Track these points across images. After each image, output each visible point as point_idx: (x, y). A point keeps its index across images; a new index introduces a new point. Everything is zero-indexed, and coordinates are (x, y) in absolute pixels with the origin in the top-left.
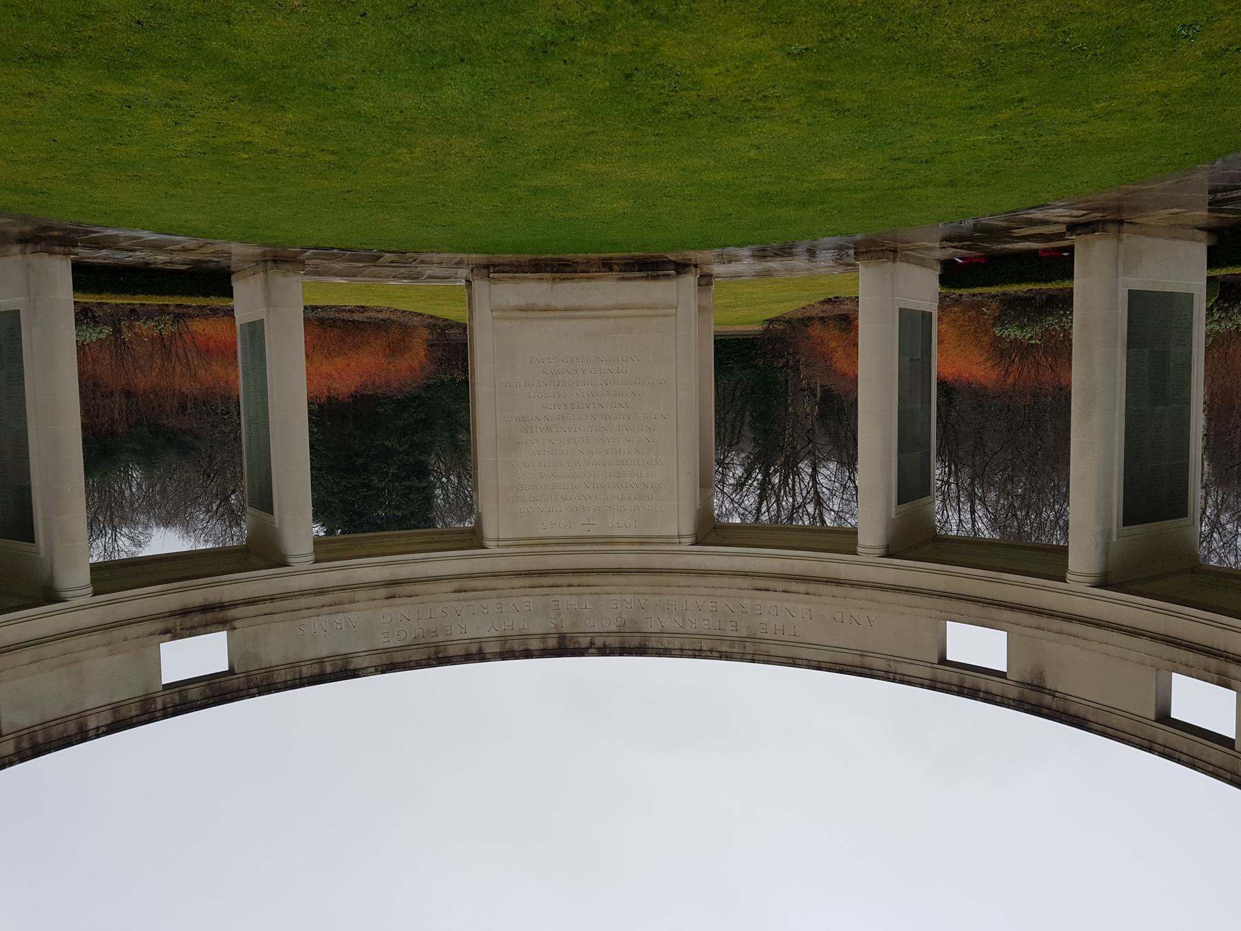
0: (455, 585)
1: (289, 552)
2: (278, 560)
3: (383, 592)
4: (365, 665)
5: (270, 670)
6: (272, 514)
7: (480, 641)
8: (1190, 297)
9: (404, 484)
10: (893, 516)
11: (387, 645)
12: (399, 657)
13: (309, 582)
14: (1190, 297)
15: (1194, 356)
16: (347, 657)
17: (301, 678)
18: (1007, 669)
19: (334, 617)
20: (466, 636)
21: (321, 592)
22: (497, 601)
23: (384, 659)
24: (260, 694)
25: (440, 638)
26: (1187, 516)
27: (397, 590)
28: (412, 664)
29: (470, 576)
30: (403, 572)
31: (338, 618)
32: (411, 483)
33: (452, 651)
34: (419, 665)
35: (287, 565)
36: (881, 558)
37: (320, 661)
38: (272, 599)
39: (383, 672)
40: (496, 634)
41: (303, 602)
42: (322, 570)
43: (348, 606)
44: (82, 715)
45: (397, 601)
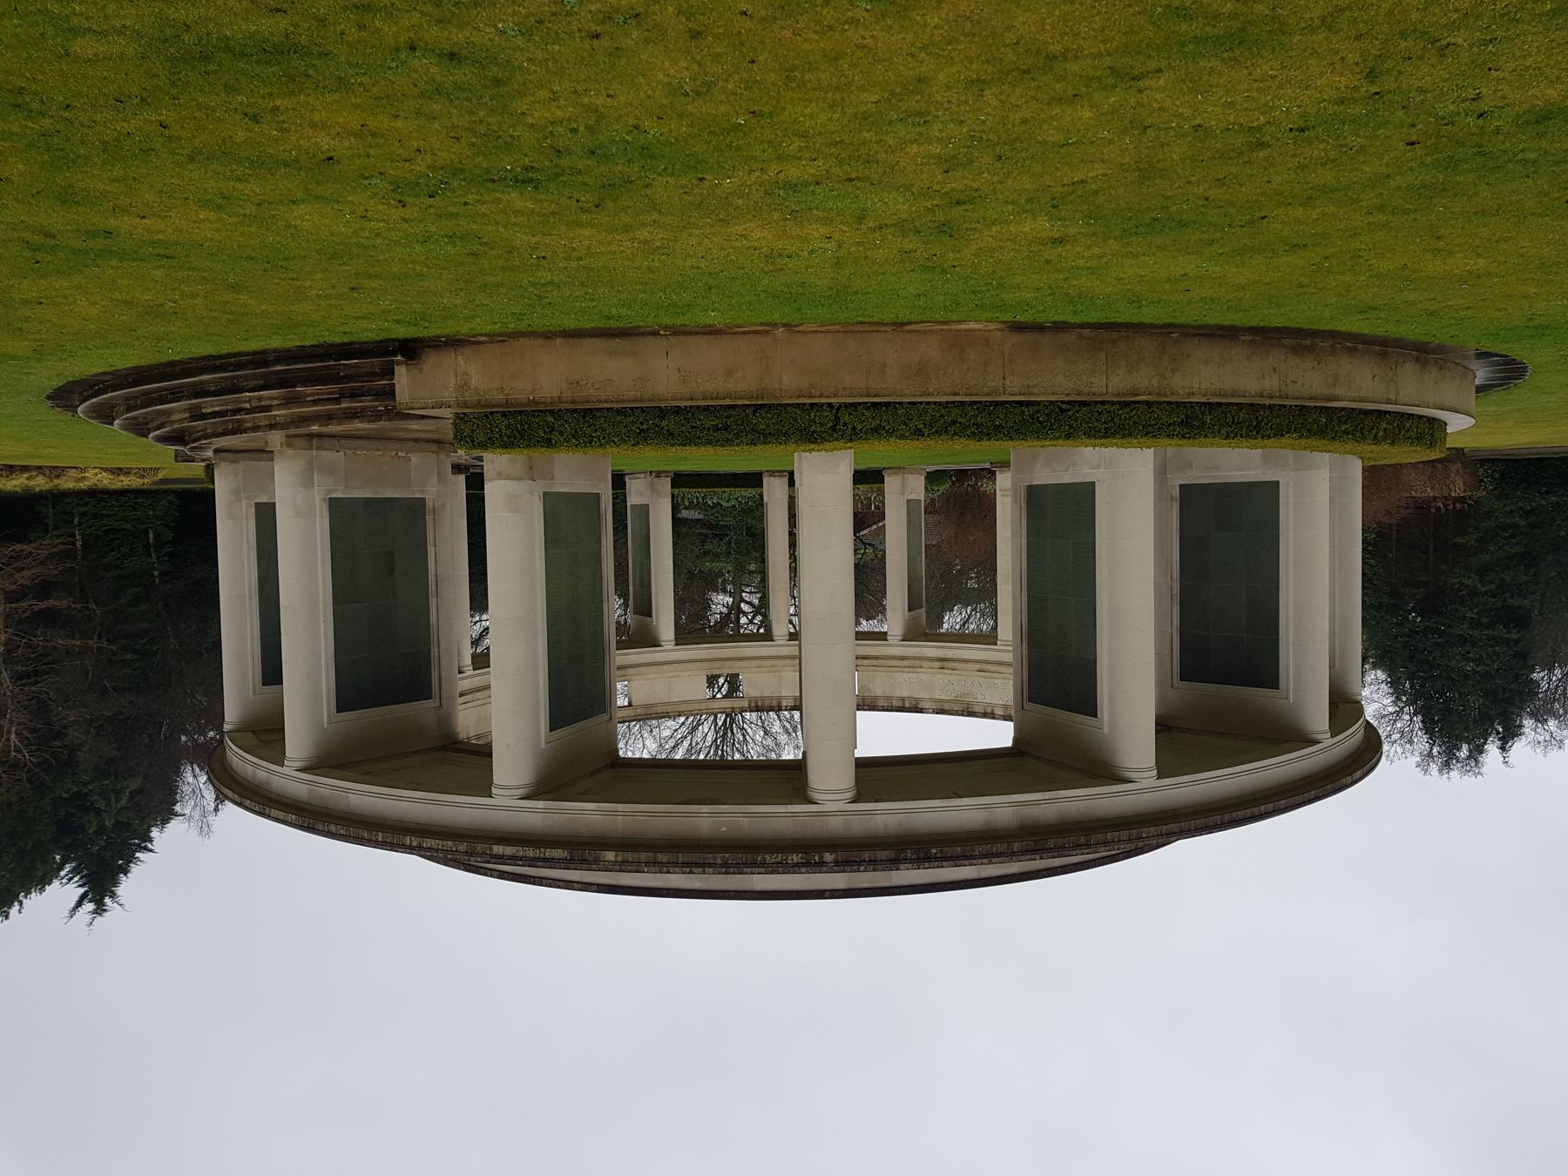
0: (978, 666)
1: (661, 639)
2: (654, 643)
3: (937, 664)
4: (927, 707)
5: (875, 698)
6: (651, 617)
7: (993, 705)
8: (597, 497)
9: (1487, 632)
10: (543, 746)
11: (940, 698)
12: (947, 706)
13: (897, 651)
14: (597, 497)
15: (603, 550)
16: (918, 700)
17: (892, 707)
18: (1457, 433)
19: (911, 675)
20: (984, 701)
21: (903, 658)
22: (1002, 681)
23: (938, 706)
24: (869, 710)
25: (970, 700)
27: (945, 664)
28: (954, 712)
29: (987, 662)
30: (949, 654)
31: (913, 675)
32: (1496, 632)
33: (977, 709)
34: (957, 713)
35: (660, 646)
36: (850, 805)
37: (903, 699)
38: (876, 658)
39: (937, 713)
40: (1001, 703)
41: (893, 663)
42: (678, 650)
43: (919, 670)
44: (779, 699)
45: (946, 671)
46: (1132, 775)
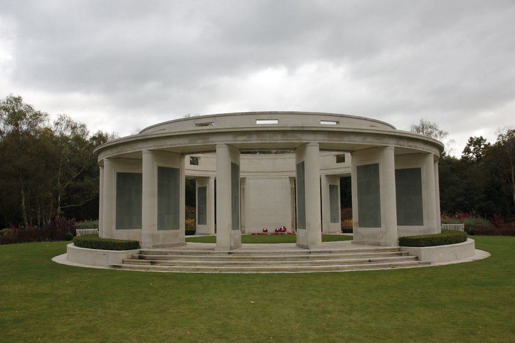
26: (357, 167)
46: (225, 146)
